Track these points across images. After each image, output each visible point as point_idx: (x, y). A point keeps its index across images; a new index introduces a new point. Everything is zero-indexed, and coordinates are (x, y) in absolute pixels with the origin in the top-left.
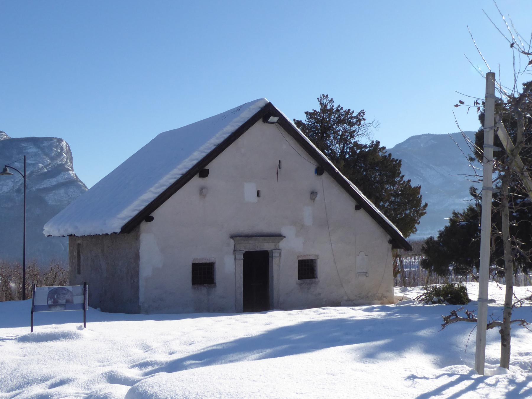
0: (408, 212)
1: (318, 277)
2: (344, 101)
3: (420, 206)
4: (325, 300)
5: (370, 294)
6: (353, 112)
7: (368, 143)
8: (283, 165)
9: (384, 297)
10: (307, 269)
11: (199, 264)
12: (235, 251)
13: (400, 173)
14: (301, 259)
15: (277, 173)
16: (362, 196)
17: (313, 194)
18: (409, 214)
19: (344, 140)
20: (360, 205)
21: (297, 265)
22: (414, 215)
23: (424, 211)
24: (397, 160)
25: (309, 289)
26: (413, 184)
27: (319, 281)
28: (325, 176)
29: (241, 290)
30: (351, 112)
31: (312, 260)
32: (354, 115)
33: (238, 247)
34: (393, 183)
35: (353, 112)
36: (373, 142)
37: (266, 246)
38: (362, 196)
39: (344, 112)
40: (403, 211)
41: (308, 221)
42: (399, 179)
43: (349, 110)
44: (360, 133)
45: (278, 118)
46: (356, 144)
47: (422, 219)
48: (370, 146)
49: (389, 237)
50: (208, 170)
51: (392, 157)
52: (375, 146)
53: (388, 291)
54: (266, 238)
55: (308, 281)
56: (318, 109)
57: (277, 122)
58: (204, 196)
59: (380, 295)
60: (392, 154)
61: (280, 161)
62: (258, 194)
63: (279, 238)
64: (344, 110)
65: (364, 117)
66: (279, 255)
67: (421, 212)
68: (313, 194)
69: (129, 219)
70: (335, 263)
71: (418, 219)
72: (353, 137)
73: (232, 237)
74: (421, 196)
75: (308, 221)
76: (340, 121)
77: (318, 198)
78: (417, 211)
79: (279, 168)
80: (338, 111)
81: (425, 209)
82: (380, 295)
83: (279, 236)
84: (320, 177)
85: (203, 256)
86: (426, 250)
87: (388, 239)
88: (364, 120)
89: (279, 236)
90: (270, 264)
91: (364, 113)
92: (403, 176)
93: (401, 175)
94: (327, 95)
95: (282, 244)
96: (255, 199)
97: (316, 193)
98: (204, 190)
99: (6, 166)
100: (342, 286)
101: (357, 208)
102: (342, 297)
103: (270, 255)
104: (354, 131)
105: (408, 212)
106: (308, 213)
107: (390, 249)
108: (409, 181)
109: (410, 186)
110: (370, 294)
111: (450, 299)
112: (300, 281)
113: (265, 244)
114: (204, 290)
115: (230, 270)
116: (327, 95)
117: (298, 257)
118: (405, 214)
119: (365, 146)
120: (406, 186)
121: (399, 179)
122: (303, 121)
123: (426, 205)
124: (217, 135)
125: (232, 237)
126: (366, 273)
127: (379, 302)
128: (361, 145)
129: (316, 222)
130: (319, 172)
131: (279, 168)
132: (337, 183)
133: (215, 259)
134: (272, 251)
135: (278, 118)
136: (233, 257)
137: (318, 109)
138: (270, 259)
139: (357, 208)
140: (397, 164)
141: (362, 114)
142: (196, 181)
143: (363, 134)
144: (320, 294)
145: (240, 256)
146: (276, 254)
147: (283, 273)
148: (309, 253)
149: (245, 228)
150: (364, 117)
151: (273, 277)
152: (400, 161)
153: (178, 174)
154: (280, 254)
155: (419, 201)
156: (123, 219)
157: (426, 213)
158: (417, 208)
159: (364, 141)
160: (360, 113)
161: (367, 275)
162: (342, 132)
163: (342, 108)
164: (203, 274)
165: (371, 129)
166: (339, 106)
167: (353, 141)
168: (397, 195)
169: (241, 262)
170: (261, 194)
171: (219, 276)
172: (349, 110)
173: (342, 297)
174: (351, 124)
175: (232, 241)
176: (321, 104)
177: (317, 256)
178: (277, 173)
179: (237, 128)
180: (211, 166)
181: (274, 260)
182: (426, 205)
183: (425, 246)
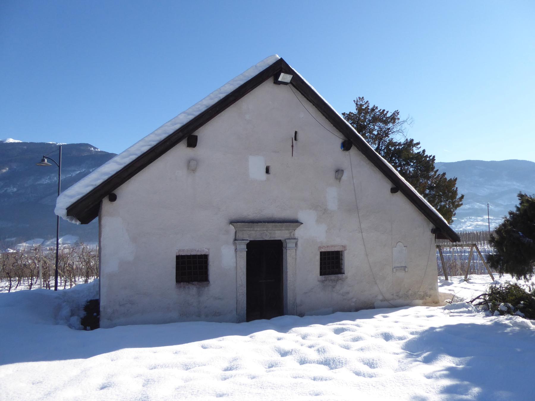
0: (443, 203)
1: (346, 273)
2: (384, 103)
3: (455, 198)
4: (354, 300)
5: (410, 292)
6: (388, 112)
7: (403, 141)
8: (299, 136)
9: (427, 296)
10: (331, 263)
11: (187, 256)
12: (235, 240)
13: (434, 168)
14: (323, 250)
15: (292, 146)
17: (339, 172)
18: (445, 206)
19: (379, 138)
20: (397, 187)
21: (318, 257)
22: (449, 207)
23: (460, 203)
24: (430, 156)
26: (448, 177)
27: (347, 278)
28: (354, 151)
30: (385, 112)
32: (389, 115)
33: (240, 235)
34: (428, 178)
36: (407, 139)
37: (278, 234)
39: (379, 111)
40: (438, 203)
41: (332, 205)
42: (433, 173)
43: (384, 110)
44: (395, 130)
45: (292, 76)
46: (391, 143)
47: (458, 211)
48: (404, 144)
49: (432, 226)
50: (197, 136)
51: (426, 154)
52: (410, 144)
53: (431, 289)
55: (333, 277)
56: (354, 111)
57: (291, 83)
58: (194, 171)
59: (422, 293)
60: (426, 150)
61: (296, 133)
62: (267, 171)
63: (295, 224)
64: (379, 109)
65: (399, 116)
66: (294, 245)
67: (457, 203)
68: (339, 172)
69: (79, 197)
70: (367, 255)
71: (454, 211)
72: (387, 135)
73: (232, 222)
74: (457, 188)
75: (332, 205)
76: (375, 120)
77: (345, 177)
78: (453, 203)
79: (296, 139)
80: (373, 110)
81: (461, 201)
82: (422, 293)
84: (347, 153)
85: (192, 246)
86: (497, 242)
87: (431, 229)
88: (399, 119)
89: (296, 222)
90: (284, 256)
91: (398, 113)
92: (437, 170)
93: (435, 170)
94: (363, 98)
95: (299, 232)
96: (263, 175)
97: (343, 171)
98: (193, 163)
99: (44, 157)
100: (376, 283)
101: (394, 191)
102: (376, 296)
103: (284, 245)
104: (389, 129)
105: (443, 203)
106: (332, 196)
107: (434, 239)
108: (444, 174)
109: (446, 179)
110: (410, 292)
111: (524, 308)
112: (323, 277)
113: (276, 232)
114: (193, 289)
115: (229, 264)
116: (363, 98)
117: (320, 248)
118: (441, 206)
119: (400, 144)
120: (441, 178)
121: (433, 173)
123: (462, 197)
125: (232, 222)
126: (405, 267)
128: (396, 142)
129: (364, 223)
130: (346, 146)
131: (296, 139)
132: (368, 161)
133: (209, 250)
134: (285, 240)
135: (292, 76)
136: (233, 248)
137: (354, 111)
138: (284, 251)
139: (394, 191)
140: (430, 160)
142: (181, 151)
144: (348, 293)
145: (243, 247)
146: (290, 244)
147: (301, 270)
148: (333, 243)
149: (250, 211)
150: (399, 116)
151: (287, 272)
152: (434, 157)
153: (154, 141)
154: (296, 244)
155: (455, 193)
156: (71, 197)
157: (462, 204)
158: (452, 200)
160: (394, 114)
161: (406, 269)
162: (378, 131)
163: (377, 108)
164: (192, 269)
165: (405, 125)
166: (374, 106)
167: (387, 139)
168: (431, 188)
169: (244, 254)
170: (271, 170)
171: (214, 270)
172: (384, 110)
173: (376, 296)
174: (386, 122)
175: (232, 227)
176: (357, 104)
177: (344, 247)
178: (292, 146)
179: (237, 86)
180: (204, 133)
181: (288, 252)
182: (462, 197)
183: (495, 235)
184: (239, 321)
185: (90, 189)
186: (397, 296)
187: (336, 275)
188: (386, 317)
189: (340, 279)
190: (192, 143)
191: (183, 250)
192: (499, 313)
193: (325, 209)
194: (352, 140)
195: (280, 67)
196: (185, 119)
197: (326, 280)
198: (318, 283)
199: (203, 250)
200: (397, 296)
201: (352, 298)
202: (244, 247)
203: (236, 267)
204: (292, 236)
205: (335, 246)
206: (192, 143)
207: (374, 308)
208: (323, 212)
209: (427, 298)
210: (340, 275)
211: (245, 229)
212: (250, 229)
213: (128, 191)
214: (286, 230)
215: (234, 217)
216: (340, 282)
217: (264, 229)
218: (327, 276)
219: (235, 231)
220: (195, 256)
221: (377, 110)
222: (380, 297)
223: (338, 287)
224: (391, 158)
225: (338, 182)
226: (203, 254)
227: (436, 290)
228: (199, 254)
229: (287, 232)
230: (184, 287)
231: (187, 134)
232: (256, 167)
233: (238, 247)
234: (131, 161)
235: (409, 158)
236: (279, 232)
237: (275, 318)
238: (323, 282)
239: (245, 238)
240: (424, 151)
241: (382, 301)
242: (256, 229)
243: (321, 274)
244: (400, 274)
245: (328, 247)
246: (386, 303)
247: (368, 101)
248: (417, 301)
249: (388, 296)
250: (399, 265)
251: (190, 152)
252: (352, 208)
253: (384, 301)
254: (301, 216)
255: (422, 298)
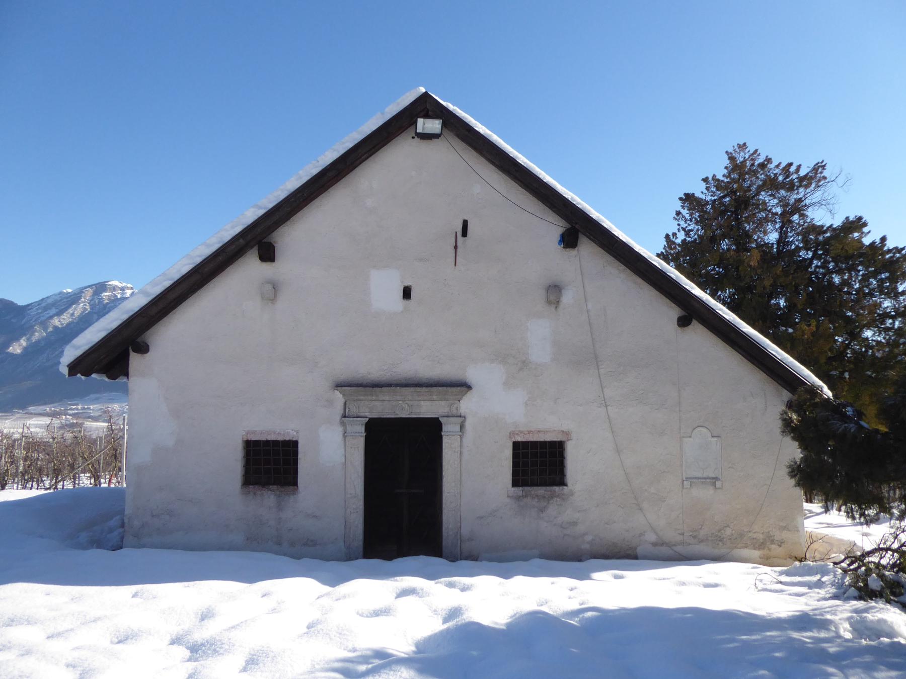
2: (782, 150)
4: (589, 538)
5: (728, 532)
6: (799, 167)
9: (772, 542)
10: (539, 464)
12: (345, 416)
14: (519, 439)
15: (456, 247)
16: (697, 291)
21: (509, 452)
25: (542, 510)
27: (572, 493)
29: (358, 503)
31: (553, 444)
33: (353, 409)
35: (799, 167)
37: (426, 407)
38: (697, 291)
39: (777, 166)
43: (791, 164)
52: (857, 224)
54: (418, 389)
55: (540, 491)
62: (407, 293)
63: (463, 389)
64: (775, 163)
66: (458, 428)
73: (340, 386)
76: (772, 184)
77: (568, 298)
80: (763, 166)
83: (464, 386)
84: (572, 252)
85: (271, 426)
89: (464, 386)
91: (823, 167)
94: (745, 144)
95: (468, 405)
100: (641, 509)
106: (539, 335)
110: (728, 532)
112: (519, 491)
113: (422, 403)
115: (334, 459)
116: (745, 144)
117: (512, 434)
122: (698, 194)
124: (301, 172)
125: (340, 386)
126: (716, 479)
127: (756, 553)
136: (340, 429)
141: (820, 170)
142: (250, 268)
143: (819, 203)
144: (575, 524)
146: (449, 428)
147: (474, 476)
148: (543, 426)
149: (371, 367)
154: (462, 427)
159: (819, 216)
161: (718, 484)
164: (271, 463)
169: (361, 442)
173: (641, 535)
175: (338, 397)
177: (567, 433)
178: (456, 247)
180: (292, 237)
184: (349, 557)
185: (103, 334)
186: (694, 537)
187: (548, 488)
188: (621, 577)
189: (558, 496)
190: (268, 254)
191: (254, 432)
192: (856, 593)
193: (524, 362)
194: (577, 226)
195: (425, 106)
196: (251, 215)
197: (526, 496)
198: (508, 500)
199: (288, 433)
200: (694, 537)
201: (585, 534)
202: (362, 429)
203: (345, 464)
204: (455, 412)
205: (545, 432)
206: (268, 254)
207: (636, 557)
208: (518, 365)
209: (773, 546)
210: (556, 488)
211: (362, 397)
212: (370, 398)
213: (170, 335)
214: (441, 400)
215: (345, 374)
216: (556, 500)
217: (398, 397)
218: (527, 488)
219: (343, 401)
220: (267, 443)
221: (771, 166)
222: (651, 537)
223: (552, 510)
224: (691, 254)
225: (553, 309)
226: (287, 439)
227: (797, 529)
228: (280, 438)
229: (443, 403)
230: (255, 494)
231: (258, 239)
232: (384, 288)
233: (349, 428)
234: (163, 289)
235: (848, 257)
236: (428, 403)
237: (400, 559)
238: (518, 498)
239: (362, 414)
240: (883, 239)
241: (655, 544)
242: (381, 398)
243: (515, 484)
244: (704, 493)
245: (529, 432)
246: (664, 550)
247: (756, 151)
248: (746, 552)
249: (670, 535)
250: (700, 475)
251: (266, 269)
252: (585, 358)
253: (662, 545)
254: (472, 375)
255: (761, 546)
